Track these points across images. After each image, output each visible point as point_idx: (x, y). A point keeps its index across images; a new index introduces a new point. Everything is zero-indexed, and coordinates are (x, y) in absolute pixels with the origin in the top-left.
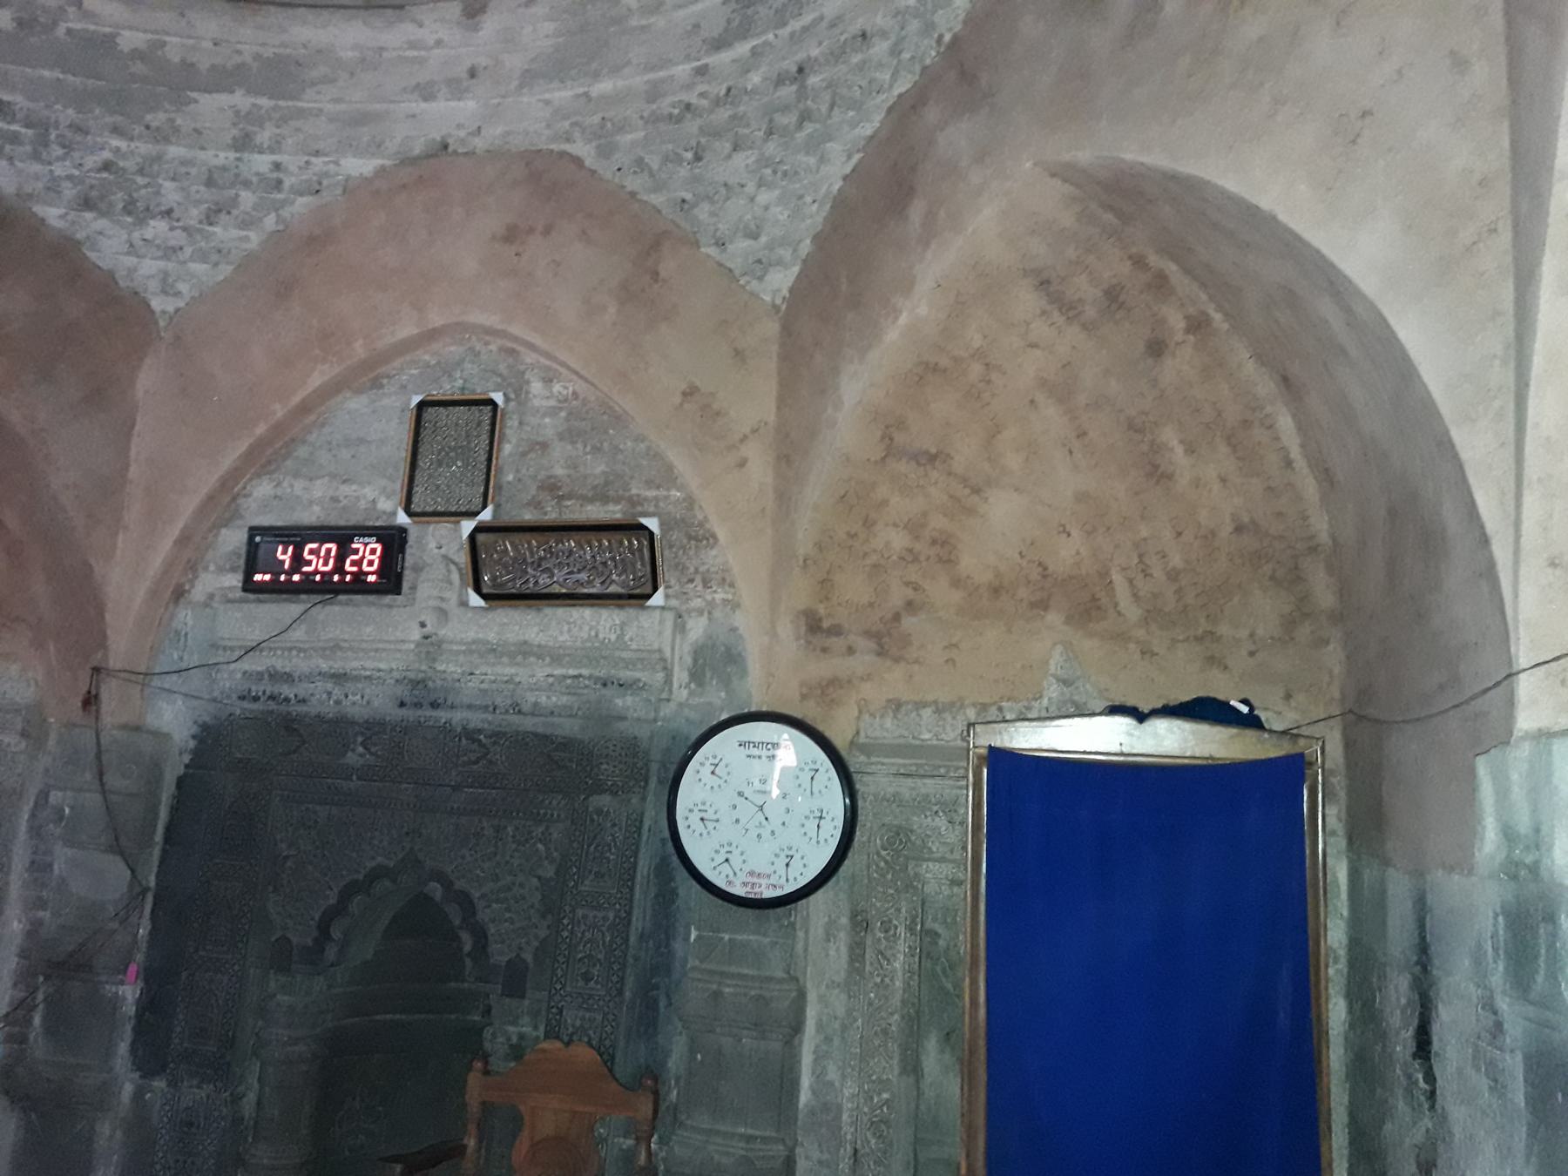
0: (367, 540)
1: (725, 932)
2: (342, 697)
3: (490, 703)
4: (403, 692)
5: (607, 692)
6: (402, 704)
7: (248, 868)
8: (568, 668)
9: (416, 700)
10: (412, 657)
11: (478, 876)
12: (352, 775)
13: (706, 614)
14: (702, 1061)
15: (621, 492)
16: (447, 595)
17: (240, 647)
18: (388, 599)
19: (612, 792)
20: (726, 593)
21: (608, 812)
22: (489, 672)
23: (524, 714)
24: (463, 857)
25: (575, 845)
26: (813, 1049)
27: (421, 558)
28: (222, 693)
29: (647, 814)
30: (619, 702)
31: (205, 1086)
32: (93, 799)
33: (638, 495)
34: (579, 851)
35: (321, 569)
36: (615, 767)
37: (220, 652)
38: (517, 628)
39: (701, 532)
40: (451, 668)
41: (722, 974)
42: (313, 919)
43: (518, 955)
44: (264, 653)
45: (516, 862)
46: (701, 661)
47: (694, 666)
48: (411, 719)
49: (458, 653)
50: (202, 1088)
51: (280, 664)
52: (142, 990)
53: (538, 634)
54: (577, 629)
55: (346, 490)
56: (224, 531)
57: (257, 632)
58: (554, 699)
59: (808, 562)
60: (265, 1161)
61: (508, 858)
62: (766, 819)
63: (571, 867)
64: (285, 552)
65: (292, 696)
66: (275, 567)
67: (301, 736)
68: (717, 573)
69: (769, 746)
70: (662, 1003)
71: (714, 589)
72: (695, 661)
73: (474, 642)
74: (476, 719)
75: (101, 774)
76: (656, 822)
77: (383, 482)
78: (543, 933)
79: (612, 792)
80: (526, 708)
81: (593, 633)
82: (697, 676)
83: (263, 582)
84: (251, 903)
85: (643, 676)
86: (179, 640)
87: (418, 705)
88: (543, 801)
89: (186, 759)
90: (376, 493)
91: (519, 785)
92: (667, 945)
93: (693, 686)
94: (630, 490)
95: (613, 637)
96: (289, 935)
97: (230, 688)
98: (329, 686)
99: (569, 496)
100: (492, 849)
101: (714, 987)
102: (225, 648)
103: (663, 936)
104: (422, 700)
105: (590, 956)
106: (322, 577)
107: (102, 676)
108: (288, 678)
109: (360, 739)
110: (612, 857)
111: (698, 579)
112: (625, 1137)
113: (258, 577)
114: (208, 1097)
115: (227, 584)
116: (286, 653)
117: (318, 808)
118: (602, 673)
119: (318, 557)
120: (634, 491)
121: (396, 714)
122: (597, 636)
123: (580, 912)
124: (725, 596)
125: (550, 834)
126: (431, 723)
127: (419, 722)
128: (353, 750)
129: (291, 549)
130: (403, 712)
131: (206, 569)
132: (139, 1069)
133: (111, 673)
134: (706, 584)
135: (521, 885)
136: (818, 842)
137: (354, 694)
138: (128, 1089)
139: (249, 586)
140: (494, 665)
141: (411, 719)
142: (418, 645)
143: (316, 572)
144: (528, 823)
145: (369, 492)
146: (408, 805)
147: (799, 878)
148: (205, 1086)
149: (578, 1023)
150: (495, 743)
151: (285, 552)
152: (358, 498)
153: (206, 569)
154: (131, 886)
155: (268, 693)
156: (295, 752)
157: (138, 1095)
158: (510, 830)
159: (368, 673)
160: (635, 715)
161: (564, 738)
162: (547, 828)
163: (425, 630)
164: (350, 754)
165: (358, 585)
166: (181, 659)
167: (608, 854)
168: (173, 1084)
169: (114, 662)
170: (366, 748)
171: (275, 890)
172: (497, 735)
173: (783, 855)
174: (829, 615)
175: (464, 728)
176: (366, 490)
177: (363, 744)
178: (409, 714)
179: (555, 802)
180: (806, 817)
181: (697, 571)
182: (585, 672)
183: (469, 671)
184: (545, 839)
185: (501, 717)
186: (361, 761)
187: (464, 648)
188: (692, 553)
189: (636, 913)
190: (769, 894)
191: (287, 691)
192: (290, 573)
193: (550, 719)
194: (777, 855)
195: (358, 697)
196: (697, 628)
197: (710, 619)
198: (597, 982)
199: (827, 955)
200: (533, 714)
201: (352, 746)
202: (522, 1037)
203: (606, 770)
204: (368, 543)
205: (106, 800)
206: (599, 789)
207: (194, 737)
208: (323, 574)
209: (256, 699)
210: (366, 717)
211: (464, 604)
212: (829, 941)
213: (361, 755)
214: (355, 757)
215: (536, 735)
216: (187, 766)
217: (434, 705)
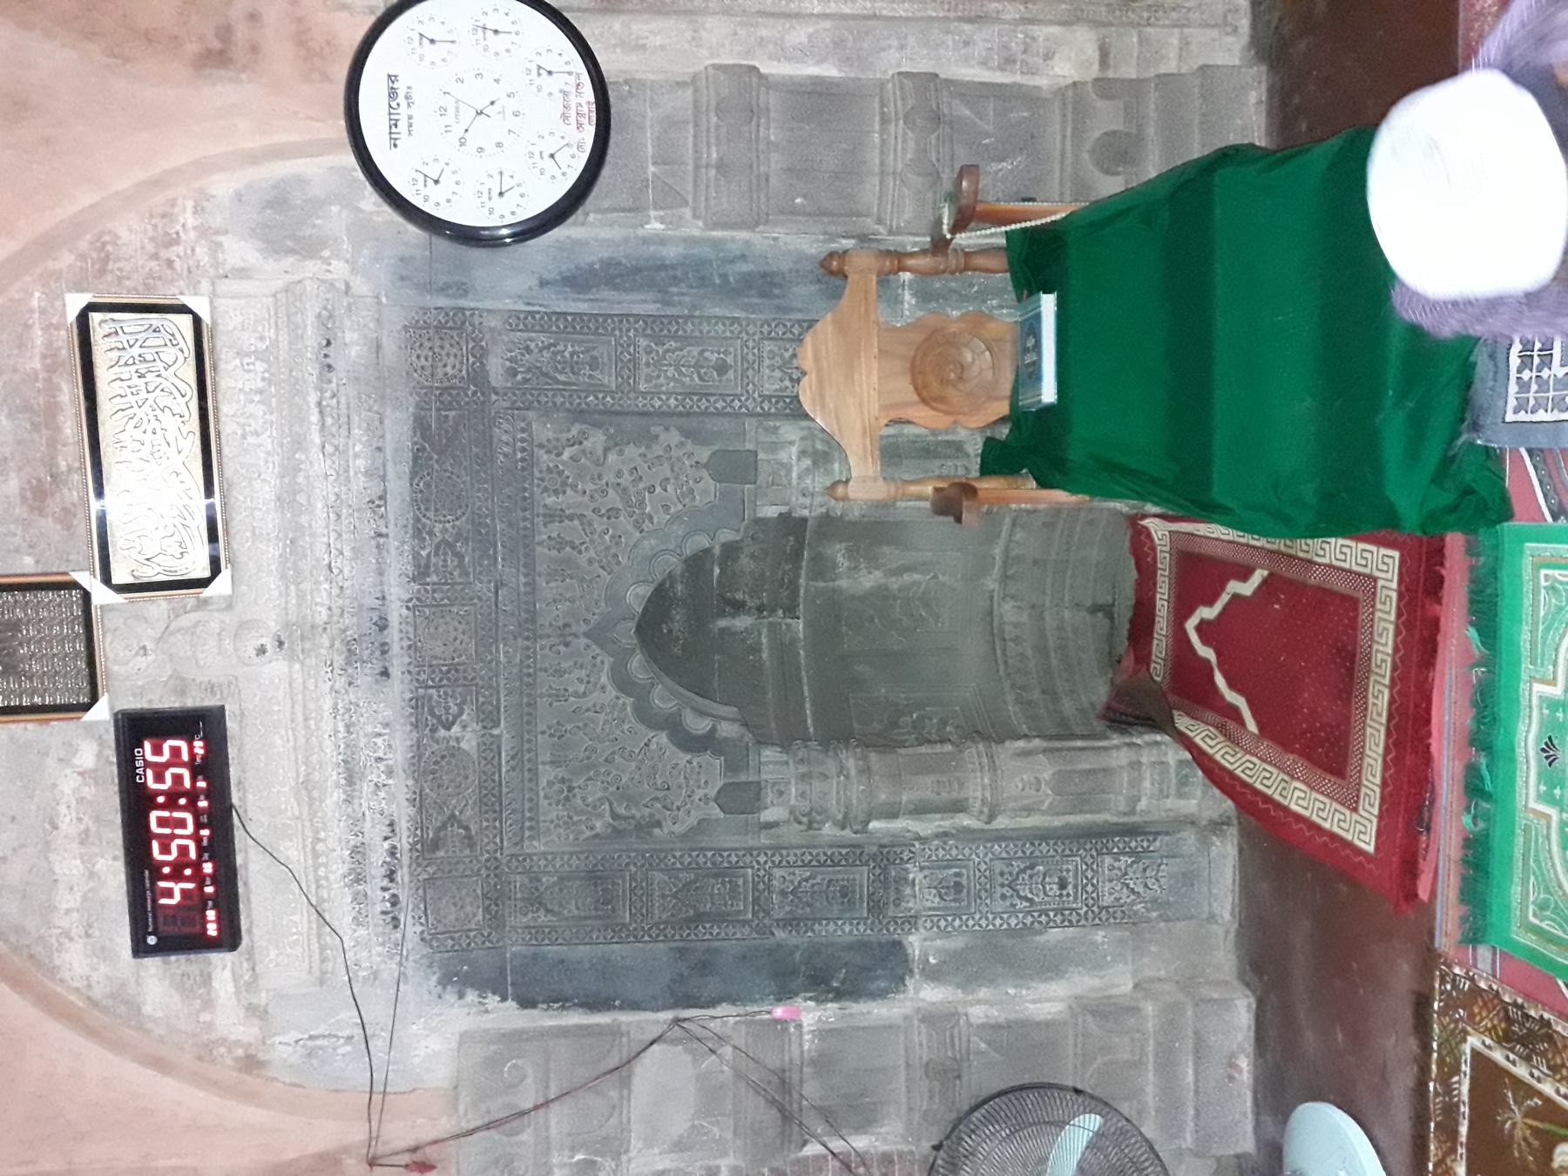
0: (140, 763)
1: (645, 170)
2: (382, 766)
3: (373, 543)
4: (365, 676)
5: (340, 365)
6: (385, 673)
7: (633, 868)
8: (310, 423)
9: (378, 653)
10: (312, 661)
11: (613, 537)
12: (492, 736)
13: (220, 238)
14: (804, 196)
15: (39, 385)
16: (214, 627)
17: (319, 936)
18: (231, 724)
19: (482, 356)
20: (184, 210)
21: (511, 360)
22: (325, 540)
23: (385, 491)
24: (590, 561)
25: (559, 400)
26: (775, 63)
27: (166, 683)
28: (391, 957)
29: (511, 307)
30: (354, 351)
31: (911, 876)
32: (557, 1120)
33: (44, 357)
34: (567, 394)
35: (190, 829)
36: (448, 355)
37: (330, 965)
38: (257, 513)
39: (95, 255)
40: (322, 597)
41: (697, 167)
42: (689, 762)
43: (706, 466)
44: (325, 896)
45: (590, 487)
46: (290, 243)
47: (297, 253)
48: (407, 660)
49: (301, 596)
50: (914, 880)
51: (338, 867)
52: (806, 999)
53: (264, 480)
54: (251, 421)
55: (67, 824)
56: (147, 1009)
57: (296, 918)
58: (358, 448)
59: (116, 51)
60: (986, 781)
61: (586, 498)
62: (492, 103)
63: (587, 404)
64: (169, 893)
65: (386, 845)
66: (195, 904)
67: (444, 826)
68: (155, 226)
69: (394, 104)
70: (745, 268)
71: (178, 227)
72: (292, 251)
73: (283, 577)
74: (398, 564)
75: (522, 1114)
76: (520, 297)
77: (51, 762)
78: (674, 437)
79: (482, 356)
80: (376, 490)
81: (257, 398)
82: (309, 248)
83: (219, 920)
84: (678, 854)
85: (312, 309)
86: (321, 1048)
87: (384, 649)
88: (506, 455)
89: (493, 1001)
90: (68, 771)
91: (486, 489)
92: (673, 267)
93: (326, 253)
94: (36, 373)
95: (260, 367)
96: (713, 793)
97: (383, 944)
98: (367, 788)
99: (51, 464)
100: (576, 522)
101: (713, 172)
102: (323, 960)
103: (663, 274)
104: (377, 644)
105: (697, 366)
106: (203, 826)
107: (381, 1149)
108: (358, 852)
109: (442, 733)
110: (570, 349)
111: (164, 254)
112: (902, 303)
113: (212, 930)
114: (922, 869)
115: (231, 988)
116: (322, 860)
117: (543, 782)
118: (312, 370)
119: (173, 837)
120: (37, 364)
121: (399, 687)
122: (261, 392)
123: (642, 387)
124: (190, 209)
125: (548, 440)
126: (411, 629)
127: (409, 647)
128: (458, 740)
129: (162, 884)
130: (396, 671)
131: (210, 1026)
132: (902, 980)
133: (372, 1139)
134: (174, 241)
135: (619, 474)
136: (517, 33)
137: (375, 747)
138: (932, 994)
139: (230, 938)
140: (313, 535)
141: (407, 660)
142: (292, 658)
143: (197, 838)
144: (537, 474)
145: (69, 785)
146: (528, 648)
147: (565, 58)
148: (911, 876)
149: (778, 374)
150: (431, 533)
151: (169, 893)
152: (80, 801)
153: (210, 1026)
154: (675, 1042)
155: (385, 883)
156: (467, 828)
157: (934, 975)
158: (550, 500)
159: (341, 728)
160: (372, 325)
161: (415, 432)
162: (541, 446)
163: (268, 647)
164: (464, 745)
165: (213, 768)
166: (350, 1038)
167: (567, 354)
168: (912, 921)
169: (357, 1133)
170: (453, 723)
171: (659, 824)
172: (419, 532)
173: (538, 81)
174: (201, 38)
175: (414, 580)
176: (67, 790)
177: (448, 727)
178: (398, 664)
179: (505, 438)
180: (485, 50)
181: (155, 256)
182: (313, 398)
183: (325, 571)
184: (556, 448)
185: (391, 526)
186: (474, 726)
187: (292, 587)
188: (127, 266)
189: (638, 309)
190: (588, 94)
191: (378, 856)
192: (199, 877)
193: (389, 454)
194: (539, 89)
195: (379, 741)
196: (239, 250)
197: (226, 232)
198: (726, 353)
199: (663, 47)
200: (384, 478)
201: (454, 743)
202: (803, 453)
203: (454, 367)
204: (144, 760)
205: (558, 1098)
206: (478, 377)
207: (461, 996)
208: (199, 826)
209: (395, 901)
210: (409, 728)
211: (229, 604)
212: (644, 47)
213: (464, 727)
214: (467, 737)
215: (413, 474)
216: (504, 999)
217: (382, 625)
